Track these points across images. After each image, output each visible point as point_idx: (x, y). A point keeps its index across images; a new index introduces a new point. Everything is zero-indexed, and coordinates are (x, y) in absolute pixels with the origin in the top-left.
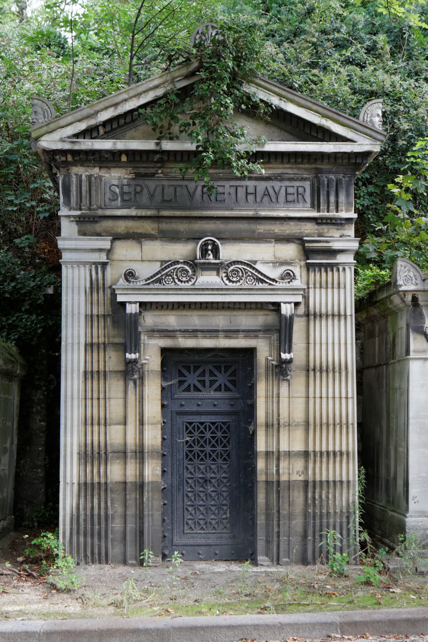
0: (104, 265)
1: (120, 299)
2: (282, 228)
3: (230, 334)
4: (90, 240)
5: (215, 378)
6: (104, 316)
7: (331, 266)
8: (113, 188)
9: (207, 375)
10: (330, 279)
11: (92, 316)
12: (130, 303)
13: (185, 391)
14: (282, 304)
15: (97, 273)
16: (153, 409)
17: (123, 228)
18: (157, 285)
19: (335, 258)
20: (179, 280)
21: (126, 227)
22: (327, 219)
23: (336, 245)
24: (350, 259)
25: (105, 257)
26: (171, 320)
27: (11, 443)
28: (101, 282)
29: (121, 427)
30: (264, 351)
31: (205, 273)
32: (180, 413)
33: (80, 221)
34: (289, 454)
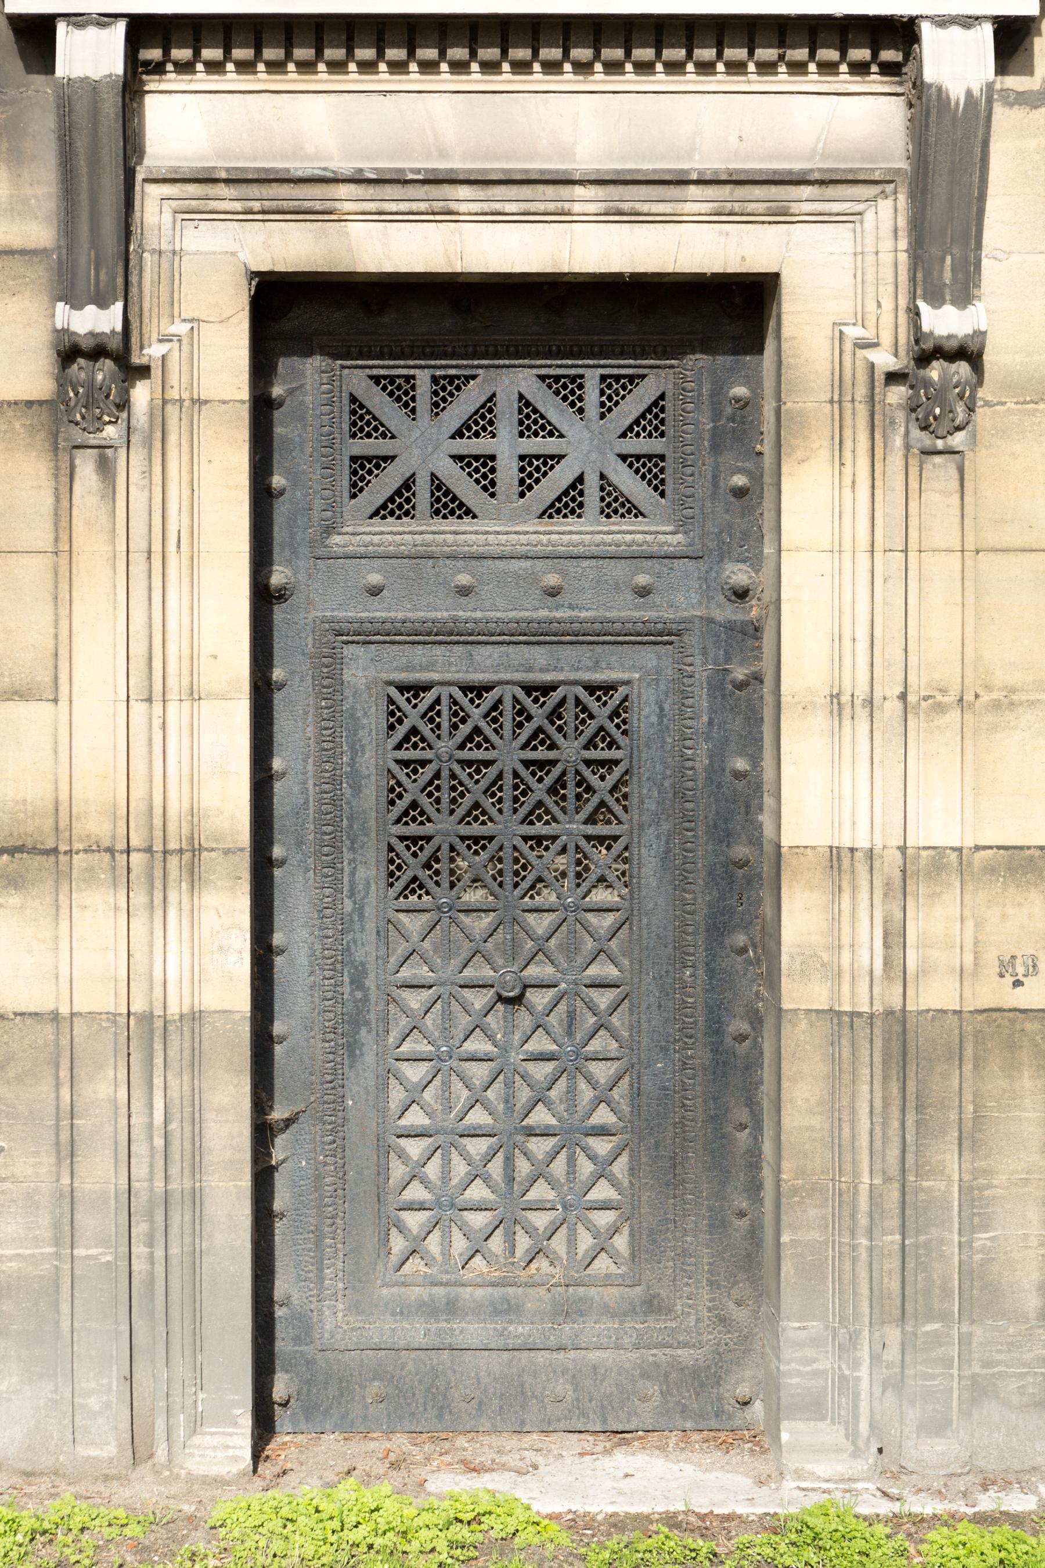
13: (381, 512)
14: (926, 29)
26: (316, 118)
30: (836, 286)
32: (367, 634)
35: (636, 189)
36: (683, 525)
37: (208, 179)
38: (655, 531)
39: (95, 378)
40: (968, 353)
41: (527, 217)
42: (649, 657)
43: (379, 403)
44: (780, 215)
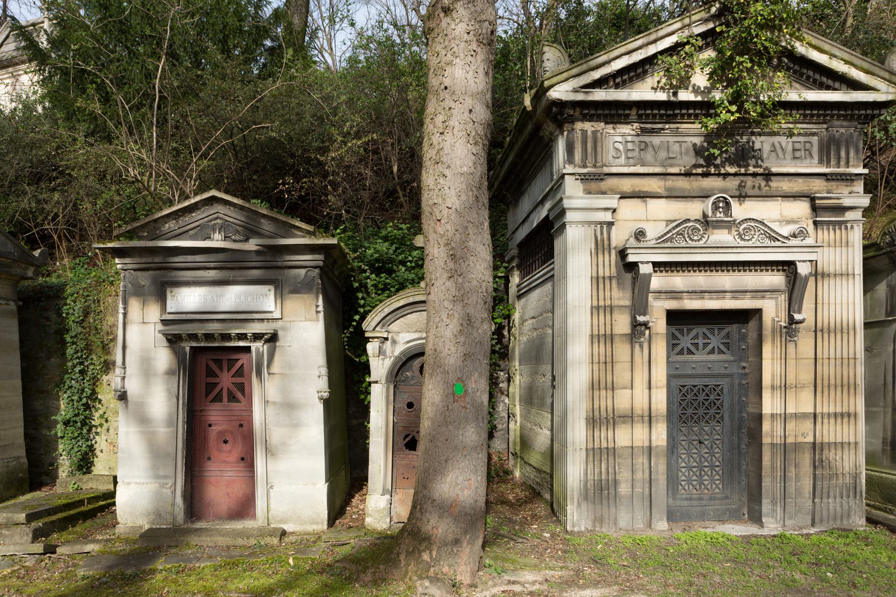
0: (610, 224)
1: (631, 258)
2: (791, 185)
3: (737, 295)
4: (597, 198)
5: (709, 341)
6: (610, 278)
7: (840, 223)
8: (617, 145)
9: (700, 338)
10: (838, 237)
11: (598, 278)
12: (642, 263)
15: (602, 233)
16: (660, 373)
17: (629, 187)
18: (669, 244)
19: (843, 215)
20: (691, 239)
21: (632, 186)
22: (836, 174)
23: (847, 202)
24: (857, 215)
25: (610, 217)
26: (679, 281)
27: (14, 363)
28: (606, 242)
29: (629, 391)
30: (773, 310)
31: (716, 231)
33: (585, 178)
34: (797, 416)
35: (738, 293)
36: (733, 355)
37: (660, 292)
38: (727, 357)
39: (638, 329)
40: (645, 325)
41: (717, 298)
42: (726, 380)
43: (677, 334)
44: (763, 297)
